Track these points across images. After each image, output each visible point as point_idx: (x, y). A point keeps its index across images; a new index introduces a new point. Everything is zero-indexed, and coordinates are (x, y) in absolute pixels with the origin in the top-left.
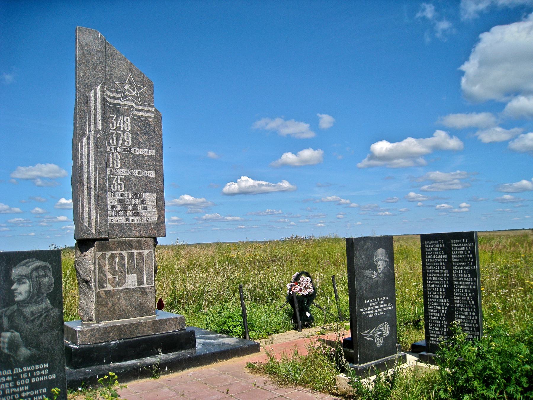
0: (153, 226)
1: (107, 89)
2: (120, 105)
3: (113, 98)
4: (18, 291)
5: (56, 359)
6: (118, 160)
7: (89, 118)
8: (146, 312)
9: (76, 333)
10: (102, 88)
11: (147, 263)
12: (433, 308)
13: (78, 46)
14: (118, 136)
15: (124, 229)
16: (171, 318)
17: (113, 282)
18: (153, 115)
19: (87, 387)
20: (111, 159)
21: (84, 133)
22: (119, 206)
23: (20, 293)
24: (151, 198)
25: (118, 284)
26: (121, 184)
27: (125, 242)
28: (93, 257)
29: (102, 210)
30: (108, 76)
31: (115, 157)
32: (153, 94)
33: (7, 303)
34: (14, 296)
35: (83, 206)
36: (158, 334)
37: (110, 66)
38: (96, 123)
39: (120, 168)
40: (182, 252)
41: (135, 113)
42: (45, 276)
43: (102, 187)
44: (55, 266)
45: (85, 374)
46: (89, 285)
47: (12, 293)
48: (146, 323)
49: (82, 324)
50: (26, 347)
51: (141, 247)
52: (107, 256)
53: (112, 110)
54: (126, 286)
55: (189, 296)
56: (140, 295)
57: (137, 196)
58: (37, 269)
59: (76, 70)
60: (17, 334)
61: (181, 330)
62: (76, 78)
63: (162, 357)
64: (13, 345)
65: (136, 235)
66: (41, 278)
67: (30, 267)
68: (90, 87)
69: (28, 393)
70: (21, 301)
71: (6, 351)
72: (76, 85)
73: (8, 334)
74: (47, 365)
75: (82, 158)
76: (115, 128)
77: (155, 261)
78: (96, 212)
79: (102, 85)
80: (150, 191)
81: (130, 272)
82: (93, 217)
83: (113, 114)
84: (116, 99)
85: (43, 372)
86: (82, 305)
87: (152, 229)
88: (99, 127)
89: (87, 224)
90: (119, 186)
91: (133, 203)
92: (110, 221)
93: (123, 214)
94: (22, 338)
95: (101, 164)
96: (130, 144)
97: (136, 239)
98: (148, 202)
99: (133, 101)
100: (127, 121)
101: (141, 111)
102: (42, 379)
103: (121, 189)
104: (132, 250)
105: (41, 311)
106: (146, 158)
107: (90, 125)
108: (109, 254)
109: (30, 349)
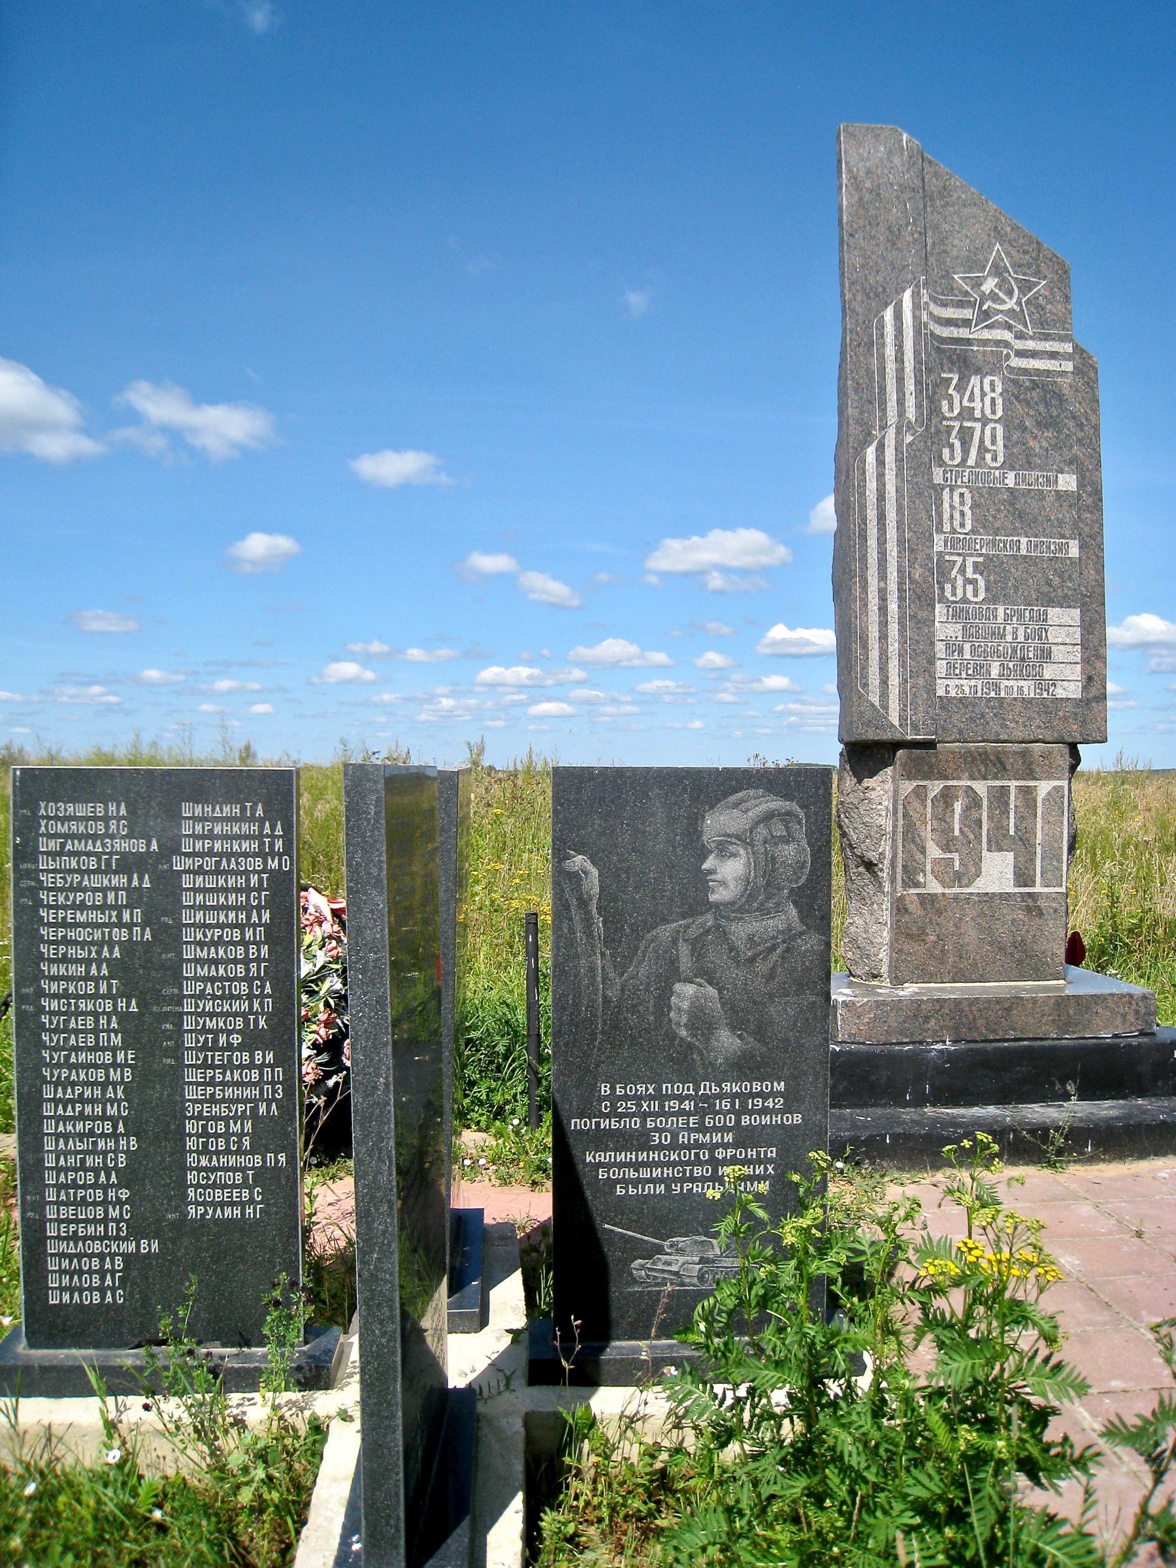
0: (1070, 708)
1: (931, 297)
2: (969, 342)
3: (949, 322)
4: (718, 877)
5: (805, 1073)
6: (967, 510)
7: (883, 389)
8: (1036, 970)
9: (835, 1007)
10: (916, 295)
11: (1046, 822)
12: (91, 1133)
13: (845, 181)
14: (965, 436)
15: (983, 716)
16: (1112, 995)
17: (944, 872)
18: (1069, 366)
19: (858, 1164)
20: (946, 505)
21: (870, 434)
22: (967, 646)
23: (723, 883)
24: (1063, 623)
25: (959, 878)
26: (974, 582)
27: (984, 756)
28: (891, 794)
29: (919, 656)
30: (932, 260)
31: (956, 498)
32: (1067, 298)
33: (691, 906)
34: (707, 889)
35: (865, 646)
36: (1069, 1039)
37: (936, 227)
38: (901, 402)
39: (973, 531)
40: (1134, 793)
41: (1016, 362)
42: (786, 840)
43: (919, 591)
44: (816, 813)
45: (855, 1125)
46: (874, 874)
47: (702, 880)
48: (1034, 1001)
49: (850, 985)
50: (733, 1029)
51: (1032, 771)
52: (931, 795)
53: (949, 359)
54: (982, 885)
55: (1160, 932)
56: (1021, 915)
57: (1021, 616)
58: (768, 817)
59: (841, 251)
60: (712, 991)
61: (1143, 1034)
62: (842, 275)
63: (1075, 1110)
64: (701, 1022)
65: (1019, 734)
66: (776, 844)
67: (750, 814)
68: (885, 296)
69: (730, 1152)
70: (726, 904)
71: (683, 1033)
72: (843, 295)
73: (690, 989)
74: (782, 1086)
75: (863, 507)
76: (956, 412)
77: (1072, 814)
78: (903, 664)
79: (917, 286)
80: (1064, 602)
81: (997, 845)
82: (894, 680)
83: (951, 371)
84: (957, 326)
85: (770, 1103)
86: (853, 929)
87: (1066, 718)
88: (911, 414)
89: (875, 699)
90: (970, 588)
91: (1009, 638)
92: (940, 692)
93: (980, 670)
94: (723, 1005)
95: (915, 521)
96: (1001, 459)
99: (1009, 327)
100: (993, 391)
101: (1034, 354)
102: (766, 1120)
103: (976, 595)
104: (1002, 778)
105: (773, 938)
106: (1051, 499)
107: (884, 410)
108: (935, 787)
109: (740, 1037)
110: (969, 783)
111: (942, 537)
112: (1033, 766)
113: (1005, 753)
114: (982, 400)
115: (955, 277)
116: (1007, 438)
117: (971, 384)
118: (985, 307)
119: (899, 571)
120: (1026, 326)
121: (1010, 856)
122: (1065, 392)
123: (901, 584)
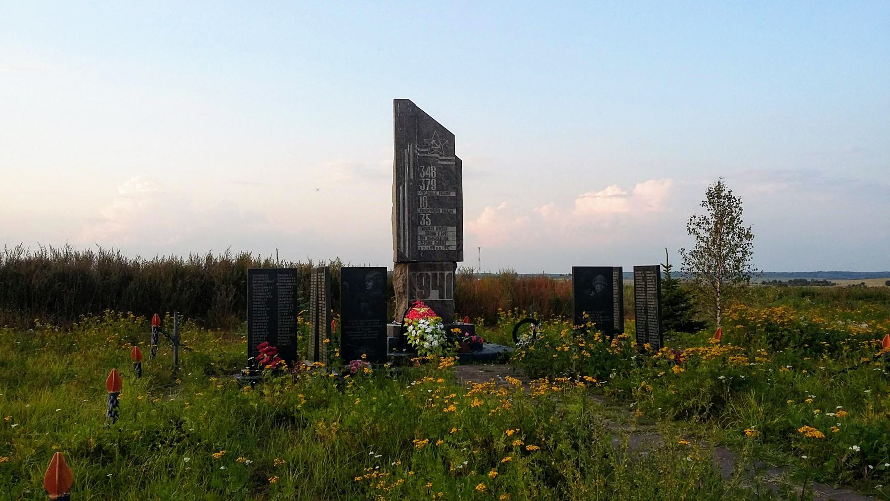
14: (426, 183)
41: (439, 162)
88: (412, 177)
98: (449, 234)
101: (445, 160)
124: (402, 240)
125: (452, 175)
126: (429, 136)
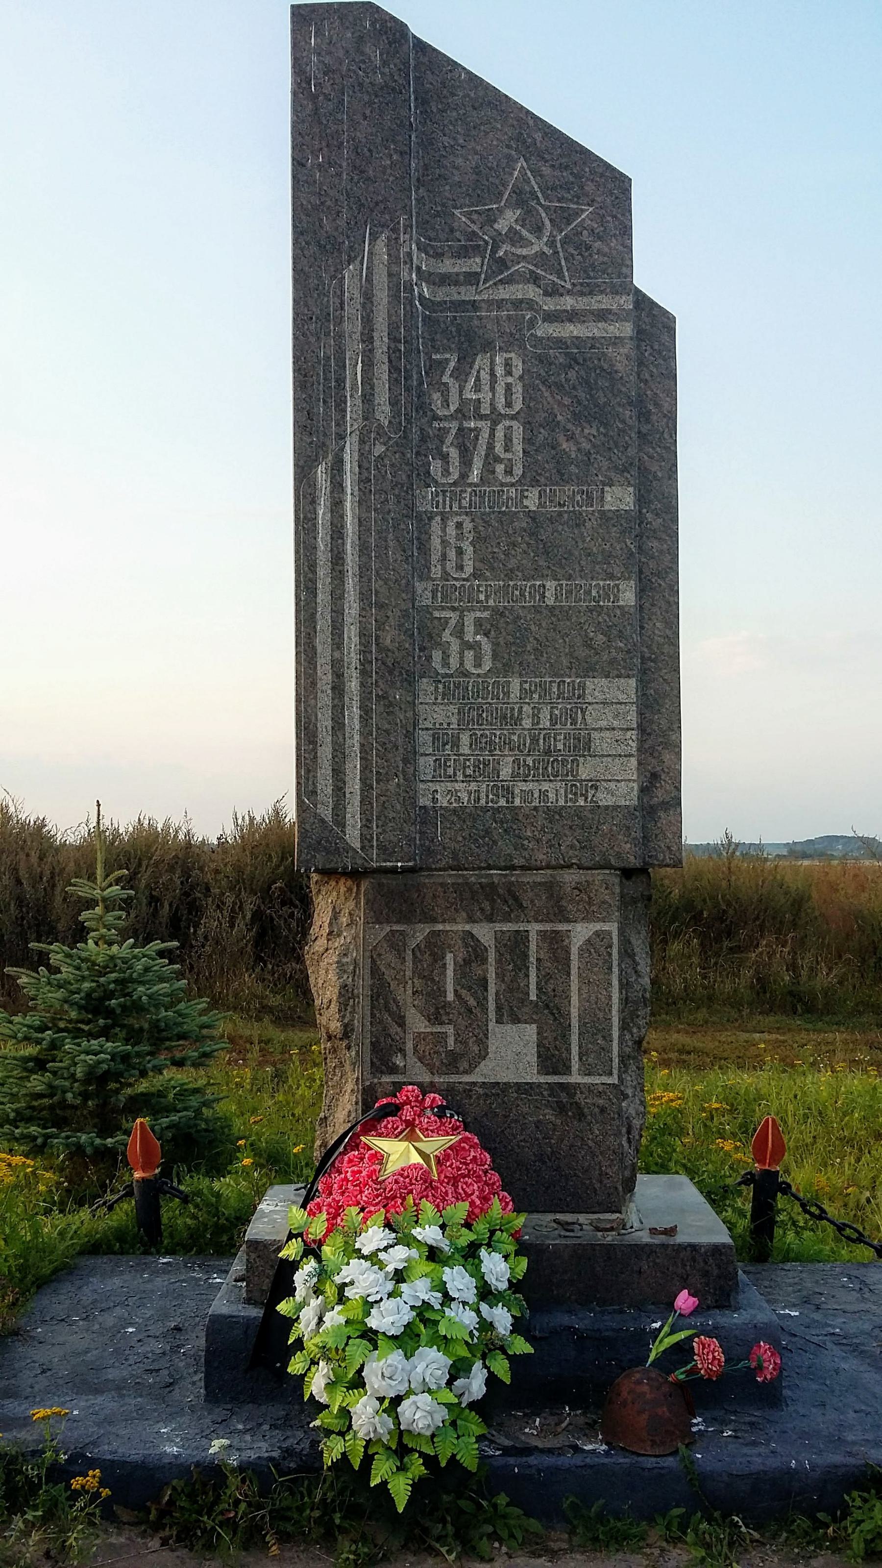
11: (584, 981)
18: (627, 329)
20: (436, 542)
22: (465, 739)
26: (475, 647)
31: (451, 530)
39: (475, 575)
41: (543, 330)
56: (549, 1115)
57: (545, 691)
79: (395, 230)
81: (510, 1014)
88: (383, 413)
90: (469, 655)
91: (527, 723)
96: (518, 471)
97: (540, 877)
98: (596, 717)
99: (535, 279)
100: (509, 373)
101: (572, 316)
103: (478, 665)
108: (420, 933)
110: (467, 927)
111: (430, 585)
112: (564, 903)
113: (521, 884)
114: (493, 389)
115: (457, 212)
116: (528, 440)
117: (476, 367)
118: (501, 253)
119: (361, 635)
120: (561, 276)
121: (531, 1030)
122: (619, 367)
123: (364, 650)
124: (325, 752)
125: (617, 400)
126: (484, 188)
